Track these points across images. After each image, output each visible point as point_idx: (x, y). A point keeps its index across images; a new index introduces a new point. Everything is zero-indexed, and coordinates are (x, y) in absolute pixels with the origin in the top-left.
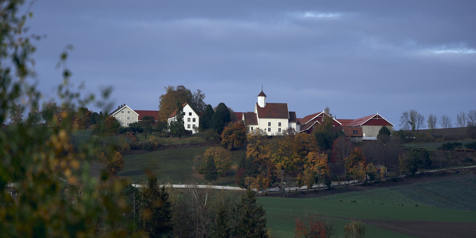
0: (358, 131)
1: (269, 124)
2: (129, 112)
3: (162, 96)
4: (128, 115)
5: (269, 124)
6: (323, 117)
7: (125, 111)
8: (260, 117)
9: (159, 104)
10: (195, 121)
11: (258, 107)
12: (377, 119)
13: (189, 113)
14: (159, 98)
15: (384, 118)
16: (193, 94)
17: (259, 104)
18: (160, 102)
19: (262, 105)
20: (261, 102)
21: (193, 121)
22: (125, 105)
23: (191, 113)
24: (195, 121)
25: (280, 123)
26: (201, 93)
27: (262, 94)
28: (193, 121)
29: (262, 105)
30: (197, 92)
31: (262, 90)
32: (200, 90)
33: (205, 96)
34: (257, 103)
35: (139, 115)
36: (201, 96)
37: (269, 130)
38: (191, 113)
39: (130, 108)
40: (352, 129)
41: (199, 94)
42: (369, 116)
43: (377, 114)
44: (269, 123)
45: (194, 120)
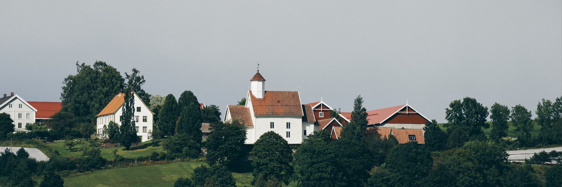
0: (416, 136)
1: (288, 125)
2: (20, 106)
3: (70, 78)
4: (20, 110)
5: (288, 125)
6: (320, 111)
7: (16, 103)
8: (257, 116)
9: (62, 91)
10: (146, 121)
11: (253, 97)
12: (407, 112)
13: (4, 94)
14: (63, 80)
15: (417, 112)
16: (124, 76)
17: (253, 93)
18: (64, 88)
19: (259, 95)
20: (257, 89)
21: (144, 121)
22: (12, 94)
23: (140, 108)
24: (146, 121)
25: (289, 123)
26: (138, 75)
27: (258, 77)
28: (144, 121)
29: (259, 95)
30: (130, 73)
31: (258, 71)
32: (137, 70)
33: (144, 81)
34: (251, 92)
35: (36, 110)
36: (138, 79)
37: (288, 134)
38: (140, 108)
39: (21, 97)
40: (406, 133)
41: (134, 76)
42: (394, 107)
43: (407, 105)
44: (271, 123)
45: (145, 120)
